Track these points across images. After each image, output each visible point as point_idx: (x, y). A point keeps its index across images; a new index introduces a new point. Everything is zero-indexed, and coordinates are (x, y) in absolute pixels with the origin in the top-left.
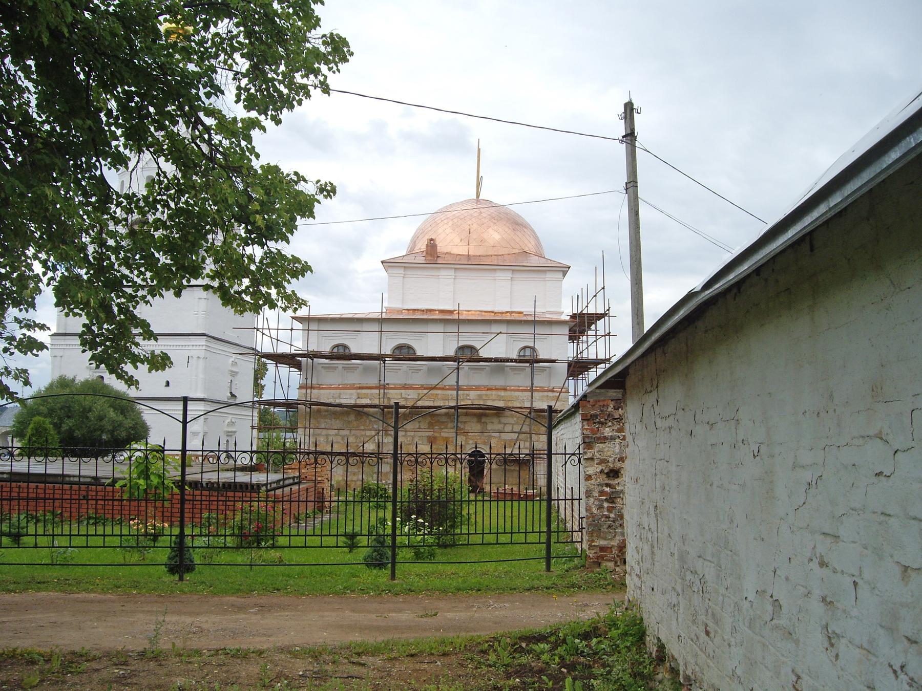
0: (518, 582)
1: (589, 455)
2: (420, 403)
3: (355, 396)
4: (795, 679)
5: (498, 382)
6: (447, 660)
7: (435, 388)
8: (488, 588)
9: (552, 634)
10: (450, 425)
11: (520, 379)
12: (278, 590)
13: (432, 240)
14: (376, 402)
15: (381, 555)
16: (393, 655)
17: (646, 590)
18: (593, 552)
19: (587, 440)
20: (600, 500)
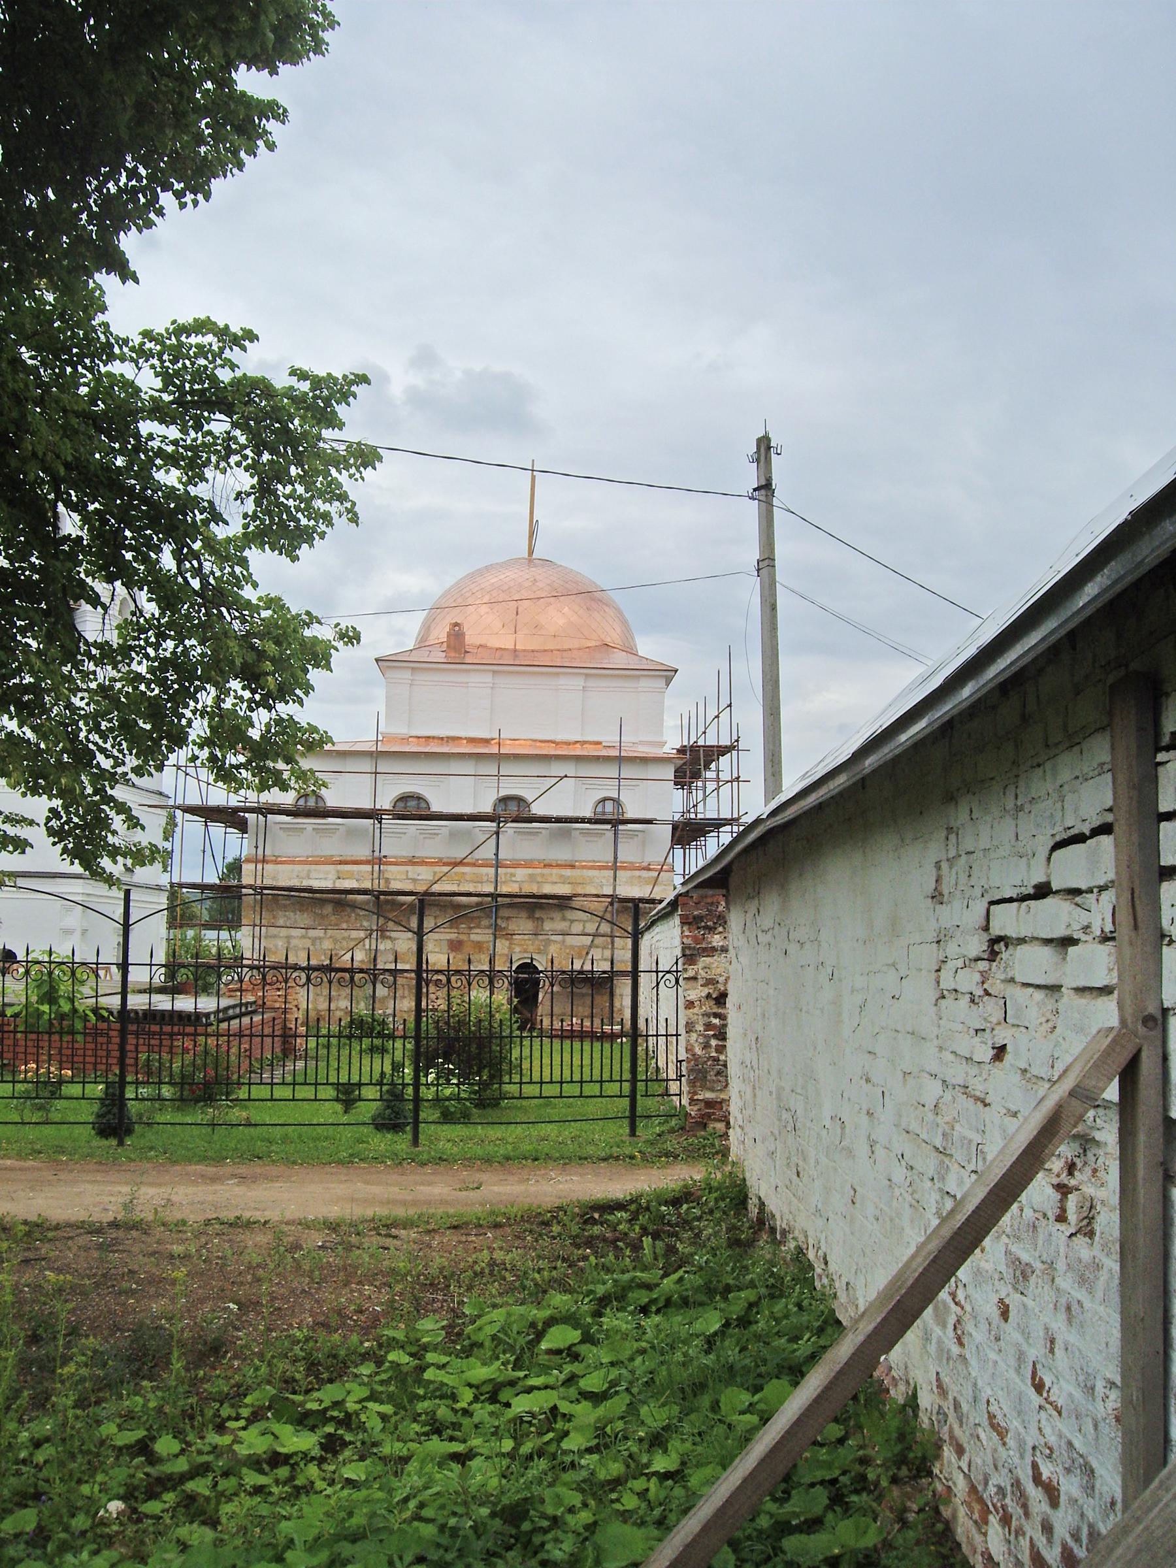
0: (590, 1150)
1: (690, 973)
2: (437, 888)
3: (332, 876)
4: (852, 1193)
5: (562, 854)
6: (499, 1232)
7: (461, 863)
8: (548, 1157)
9: (632, 1201)
10: (485, 922)
11: (595, 847)
12: (259, 1158)
13: (456, 624)
14: (367, 885)
15: (397, 1113)
16: (430, 1227)
17: (749, 1142)
18: (696, 1108)
19: (688, 952)
20: (705, 1036)
